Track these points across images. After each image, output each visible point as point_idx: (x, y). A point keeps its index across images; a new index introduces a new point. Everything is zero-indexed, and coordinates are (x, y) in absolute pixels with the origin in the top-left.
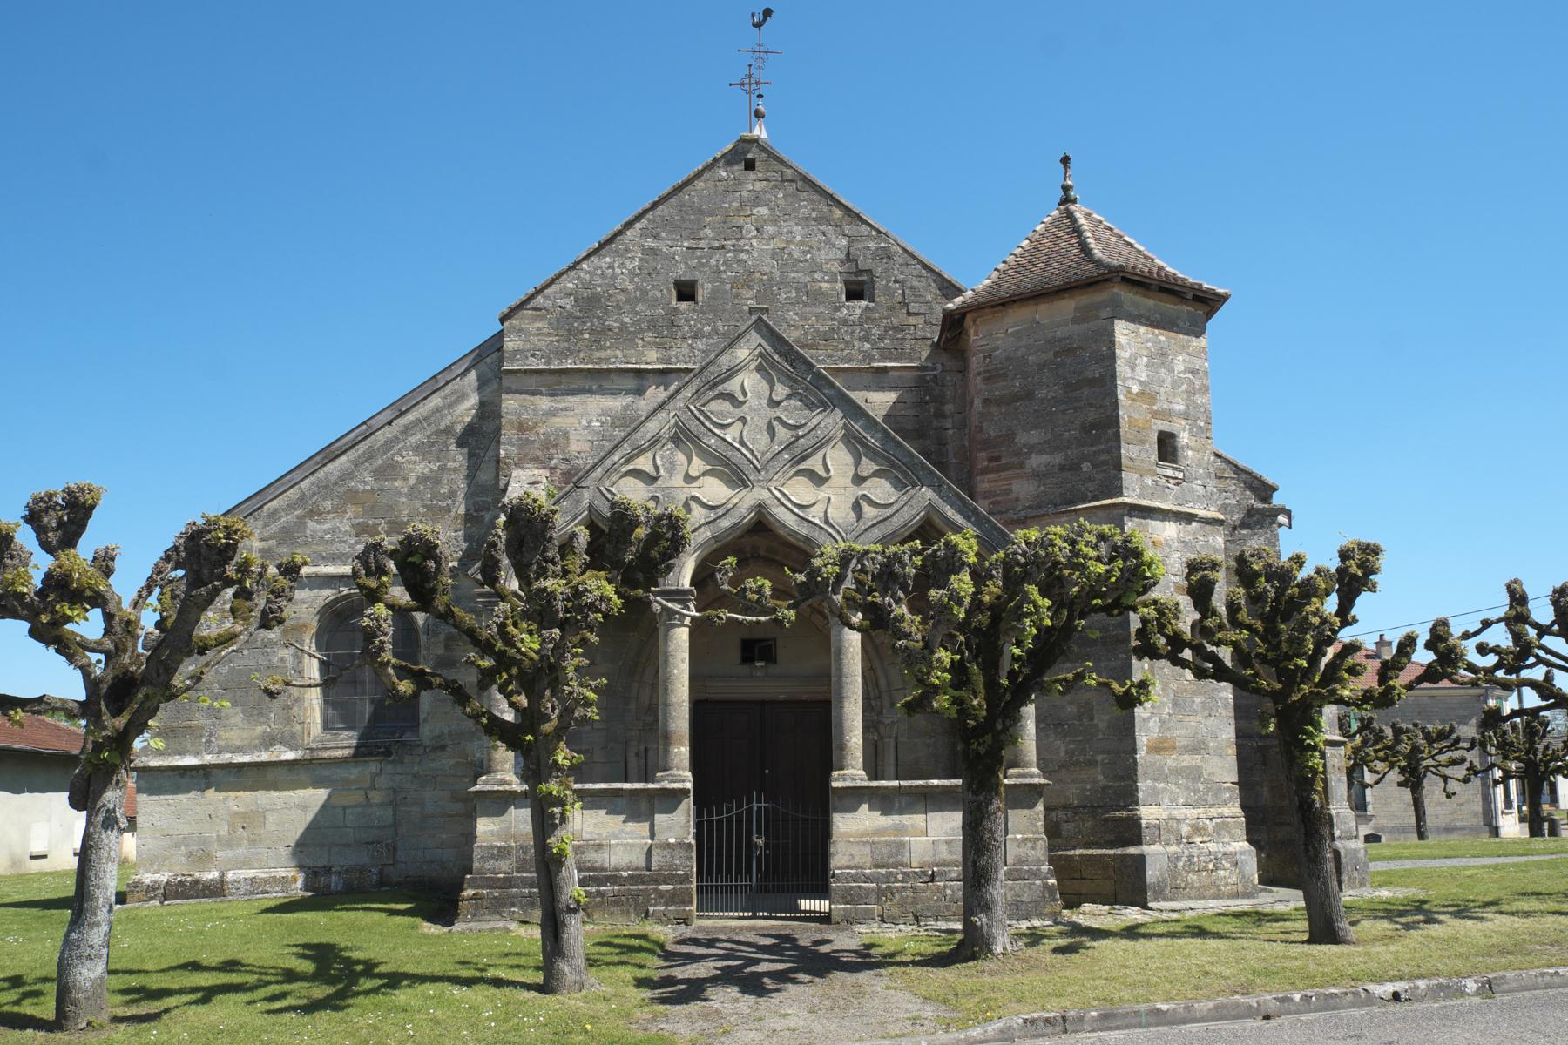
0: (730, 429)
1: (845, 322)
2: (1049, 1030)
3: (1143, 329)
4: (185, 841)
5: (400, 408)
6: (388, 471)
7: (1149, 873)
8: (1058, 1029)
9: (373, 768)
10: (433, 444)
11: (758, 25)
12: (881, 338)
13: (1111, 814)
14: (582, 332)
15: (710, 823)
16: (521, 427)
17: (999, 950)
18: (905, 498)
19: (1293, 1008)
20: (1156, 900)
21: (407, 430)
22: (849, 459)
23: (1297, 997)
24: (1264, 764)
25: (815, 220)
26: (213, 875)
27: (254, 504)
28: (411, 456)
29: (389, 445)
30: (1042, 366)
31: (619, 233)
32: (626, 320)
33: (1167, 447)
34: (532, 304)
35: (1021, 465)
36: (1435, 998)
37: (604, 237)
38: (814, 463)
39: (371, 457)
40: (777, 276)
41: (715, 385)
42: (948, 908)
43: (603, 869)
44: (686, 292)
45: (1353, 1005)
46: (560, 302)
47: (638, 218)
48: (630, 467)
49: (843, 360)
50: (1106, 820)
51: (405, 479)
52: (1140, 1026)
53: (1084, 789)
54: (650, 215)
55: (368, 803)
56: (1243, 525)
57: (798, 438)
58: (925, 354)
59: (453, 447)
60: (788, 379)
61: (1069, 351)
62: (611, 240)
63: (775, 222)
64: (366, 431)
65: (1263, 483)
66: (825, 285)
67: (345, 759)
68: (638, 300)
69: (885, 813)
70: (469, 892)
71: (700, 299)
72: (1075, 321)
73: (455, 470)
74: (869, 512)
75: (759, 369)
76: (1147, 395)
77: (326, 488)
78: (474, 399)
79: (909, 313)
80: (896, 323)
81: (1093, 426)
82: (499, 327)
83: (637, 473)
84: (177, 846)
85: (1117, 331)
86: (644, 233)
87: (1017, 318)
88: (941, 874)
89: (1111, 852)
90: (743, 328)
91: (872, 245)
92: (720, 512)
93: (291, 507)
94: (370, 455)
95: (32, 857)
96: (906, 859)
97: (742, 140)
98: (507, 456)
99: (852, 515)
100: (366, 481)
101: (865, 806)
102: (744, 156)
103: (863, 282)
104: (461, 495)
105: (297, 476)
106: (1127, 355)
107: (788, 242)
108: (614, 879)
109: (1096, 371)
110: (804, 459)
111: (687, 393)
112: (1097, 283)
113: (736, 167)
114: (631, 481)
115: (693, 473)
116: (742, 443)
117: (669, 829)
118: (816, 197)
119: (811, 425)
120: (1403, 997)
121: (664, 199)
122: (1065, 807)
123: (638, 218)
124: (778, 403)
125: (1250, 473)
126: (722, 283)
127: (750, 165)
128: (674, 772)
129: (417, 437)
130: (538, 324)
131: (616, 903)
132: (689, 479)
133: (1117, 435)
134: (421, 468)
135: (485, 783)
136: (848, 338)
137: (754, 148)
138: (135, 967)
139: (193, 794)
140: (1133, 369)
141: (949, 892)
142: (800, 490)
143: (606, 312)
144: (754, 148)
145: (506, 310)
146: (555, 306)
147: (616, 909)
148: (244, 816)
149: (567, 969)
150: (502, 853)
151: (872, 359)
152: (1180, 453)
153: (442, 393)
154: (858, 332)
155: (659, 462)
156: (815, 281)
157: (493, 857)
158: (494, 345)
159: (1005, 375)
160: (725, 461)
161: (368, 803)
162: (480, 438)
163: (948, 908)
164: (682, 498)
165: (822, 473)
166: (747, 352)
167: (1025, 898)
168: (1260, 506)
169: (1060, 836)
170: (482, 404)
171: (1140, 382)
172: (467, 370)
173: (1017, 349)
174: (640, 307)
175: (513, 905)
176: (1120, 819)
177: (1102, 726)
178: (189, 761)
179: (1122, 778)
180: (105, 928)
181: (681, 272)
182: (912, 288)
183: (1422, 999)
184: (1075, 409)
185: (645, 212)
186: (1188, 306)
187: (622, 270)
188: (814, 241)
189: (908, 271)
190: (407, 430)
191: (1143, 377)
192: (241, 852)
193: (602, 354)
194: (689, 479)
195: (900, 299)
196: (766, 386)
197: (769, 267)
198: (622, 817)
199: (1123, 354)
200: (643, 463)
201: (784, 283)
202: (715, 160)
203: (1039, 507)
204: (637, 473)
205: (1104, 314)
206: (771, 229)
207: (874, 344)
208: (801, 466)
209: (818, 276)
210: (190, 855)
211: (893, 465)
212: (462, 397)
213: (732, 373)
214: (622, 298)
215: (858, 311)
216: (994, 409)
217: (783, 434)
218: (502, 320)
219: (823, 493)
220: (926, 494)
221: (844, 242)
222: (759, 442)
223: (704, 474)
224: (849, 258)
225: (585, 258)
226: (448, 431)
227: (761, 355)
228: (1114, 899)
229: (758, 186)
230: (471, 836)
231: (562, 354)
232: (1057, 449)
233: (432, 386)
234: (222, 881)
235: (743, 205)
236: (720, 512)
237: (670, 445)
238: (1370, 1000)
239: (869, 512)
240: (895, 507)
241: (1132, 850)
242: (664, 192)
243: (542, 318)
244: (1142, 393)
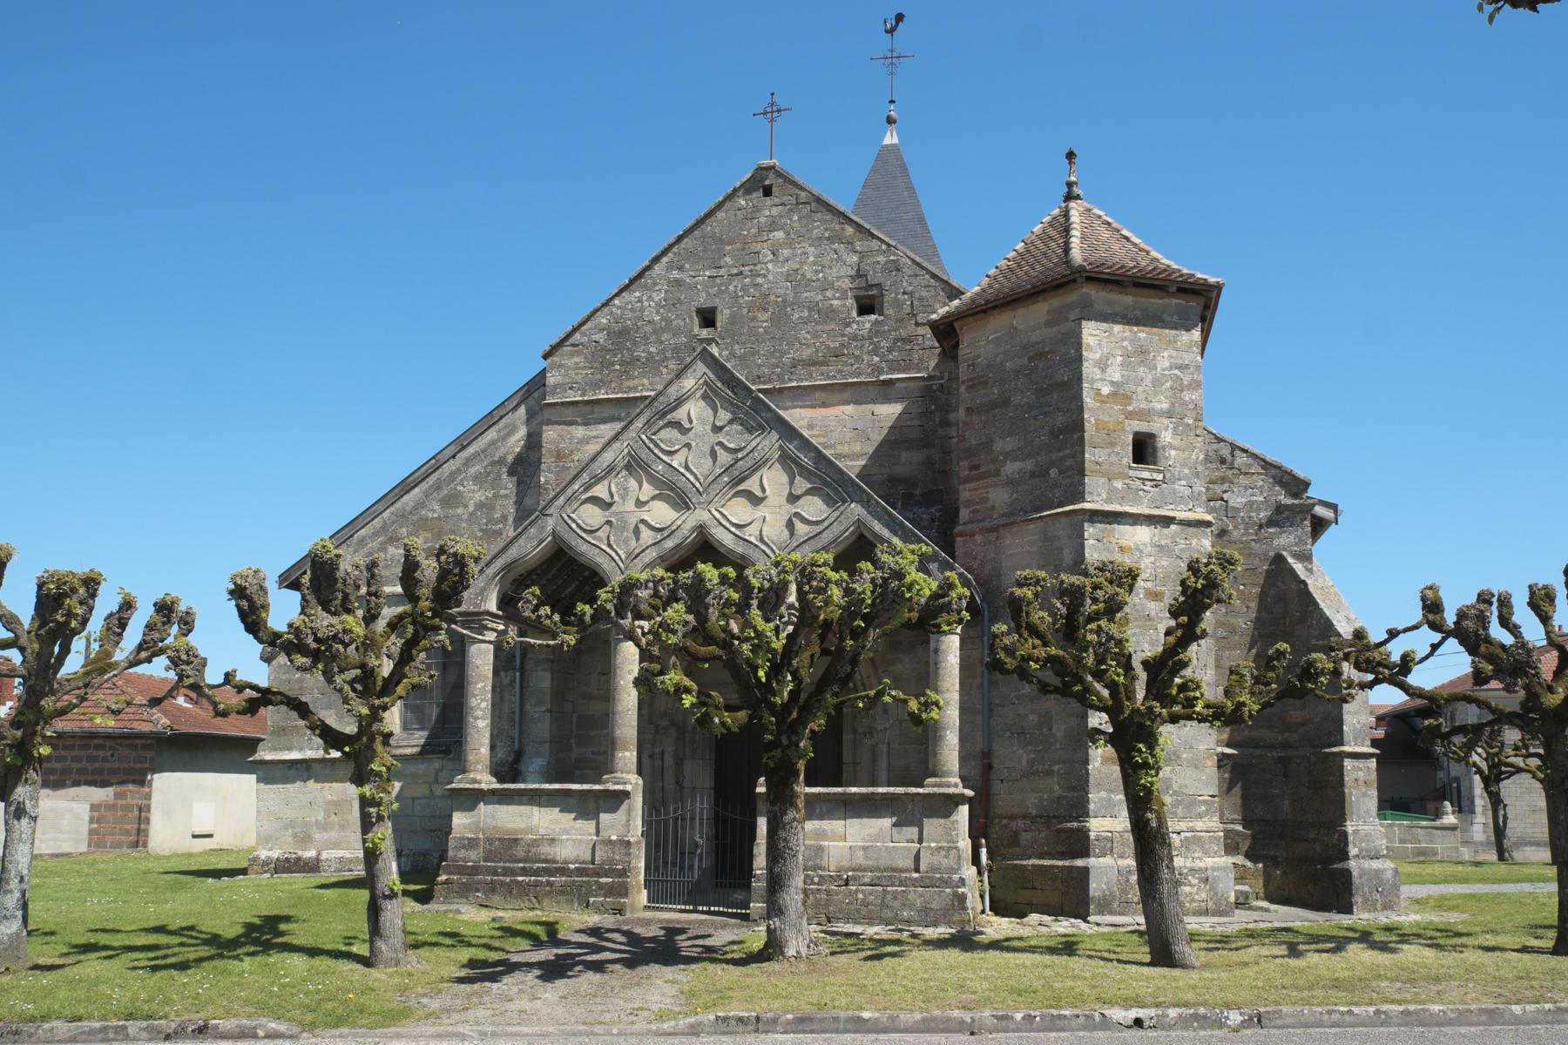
0: (677, 456)
1: (855, 338)
2: (741, 1028)
3: (1117, 328)
4: (291, 824)
5: (462, 442)
6: (453, 500)
7: (1093, 886)
8: (750, 1028)
9: (437, 764)
10: (488, 474)
11: (891, 31)
12: (890, 351)
13: (1064, 825)
14: (613, 364)
15: (658, 822)
16: (559, 456)
17: (791, 952)
18: (836, 514)
19: (1011, 1026)
20: (1101, 913)
21: (467, 463)
22: (785, 479)
23: (1019, 1016)
24: (1286, 775)
25: (828, 239)
26: (310, 854)
27: (344, 535)
28: (471, 486)
29: (453, 476)
30: (1017, 372)
31: (648, 268)
32: (653, 349)
33: (1144, 449)
34: (571, 341)
35: (997, 473)
36: (1185, 1028)
37: (634, 273)
38: (751, 485)
39: (439, 488)
40: (790, 298)
41: (664, 415)
42: (858, 911)
43: (555, 862)
44: (707, 318)
45: (1084, 1028)
46: (595, 337)
47: (664, 252)
48: (589, 494)
49: (852, 375)
50: (1059, 831)
51: (466, 506)
52: (837, 1031)
53: (1041, 799)
54: (675, 249)
55: (432, 796)
56: (1271, 522)
57: (737, 460)
58: (933, 364)
59: (504, 476)
60: (729, 405)
61: (1041, 355)
62: (640, 275)
63: (790, 245)
64: (435, 464)
65: (1295, 478)
66: (835, 303)
67: (413, 756)
68: (663, 330)
70: (443, 878)
71: (719, 324)
72: (1048, 324)
73: (506, 496)
74: (801, 529)
75: (705, 397)
76: (1120, 395)
77: (402, 517)
78: (522, 432)
79: (917, 324)
80: (904, 333)
81: (1061, 431)
82: (544, 364)
83: (595, 500)
84: (286, 828)
85: (1085, 332)
86: (670, 268)
87: (997, 324)
88: (855, 878)
89: (1060, 863)
90: (688, 360)
91: (881, 259)
92: (666, 533)
93: (375, 534)
94: (437, 487)
95: (194, 836)
96: (824, 863)
97: (760, 169)
98: (547, 483)
99: (786, 532)
100: (435, 510)
102: (762, 183)
103: (873, 297)
104: (511, 519)
105: (380, 507)
106: (1097, 356)
107: (802, 263)
108: (562, 871)
109: (1064, 375)
110: (742, 480)
111: (639, 424)
112: (1044, 291)
113: (755, 195)
114: (589, 507)
115: (643, 499)
116: (687, 468)
117: (612, 827)
118: (829, 217)
119: (749, 448)
120: (1146, 1024)
121: (688, 232)
122: (1024, 817)
123: (664, 252)
124: (721, 428)
125: (1280, 468)
126: (740, 308)
127: (768, 192)
128: (618, 775)
129: (476, 469)
130: (576, 359)
131: (562, 893)
132: (640, 504)
133: (1082, 438)
134: (479, 496)
135: (460, 781)
136: (857, 353)
137: (772, 175)
138: (110, 926)
139: (298, 784)
140: (1103, 371)
141: (860, 896)
142: (738, 511)
143: (635, 344)
144: (772, 175)
145: (547, 348)
146: (590, 341)
147: (562, 898)
148: (336, 804)
149: (384, 947)
150: (472, 843)
151: (881, 371)
152: (1160, 454)
153: (496, 427)
154: (868, 346)
155: (614, 489)
156: (826, 299)
157: (464, 847)
158: (537, 384)
159: (986, 383)
160: (671, 486)
161: (432, 796)
162: (525, 466)
163: (858, 911)
164: (633, 520)
165: (759, 493)
166: (693, 382)
168: (1289, 501)
169: (1018, 845)
170: (530, 435)
171: (1112, 383)
172: (518, 405)
173: (996, 356)
174: (665, 337)
176: (1071, 830)
177: (1059, 735)
178: (295, 755)
179: (1074, 789)
180: (17, 895)
181: (703, 301)
182: (921, 299)
183: (1170, 1027)
184: (1045, 414)
185: (671, 246)
186: (1192, 302)
187: (649, 303)
188: (826, 261)
189: (916, 282)
190: (467, 463)
191: (1117, 377)
192: (333, 834)
193: (631, 383)
194: (640, 504)
195: (908, 310)
196: (711, 412)
197: (784, 289)
198: (573, 815)
199: (1091, 356)
200: (600, 491)
201: (798, 304)
202: (735, 190)
203: (1012, 514)
204: (595, 500)
205: (1073, 316)
206: (786, 252)
207: (882, 357)
208: (740, 488)
209: (829, 294)
210: (295, 835)
211: (826, 484)
212: (514, 429)
213: (680, 402)
214: (649, 329)
215: (868, 325)
216: (975, 418)
217: (725, 458)
218: (545, 357)
219: (759, 512)
220: (856, 510)
221: (855, 259)
222: (702, 466)
223: (653, 498)
224: (860, 274)
225: (617, 295)
226: (501, 462)
227: (706, 383)
228: (1058, 911)
229: (775, 211)
230: (448, 830)
231: (597, 385)
232: (1029, 455)
233: (489, 421)
234: (318, 859)
235: (760, 231)
236: (666, 533)
237: (624, 473)
238: (1106, 1023)
239: (801, 529)
240: (826, 524)
241: (1080, 863)
242: (688, 225)
243: (579, 353)
244: (1114, 395)
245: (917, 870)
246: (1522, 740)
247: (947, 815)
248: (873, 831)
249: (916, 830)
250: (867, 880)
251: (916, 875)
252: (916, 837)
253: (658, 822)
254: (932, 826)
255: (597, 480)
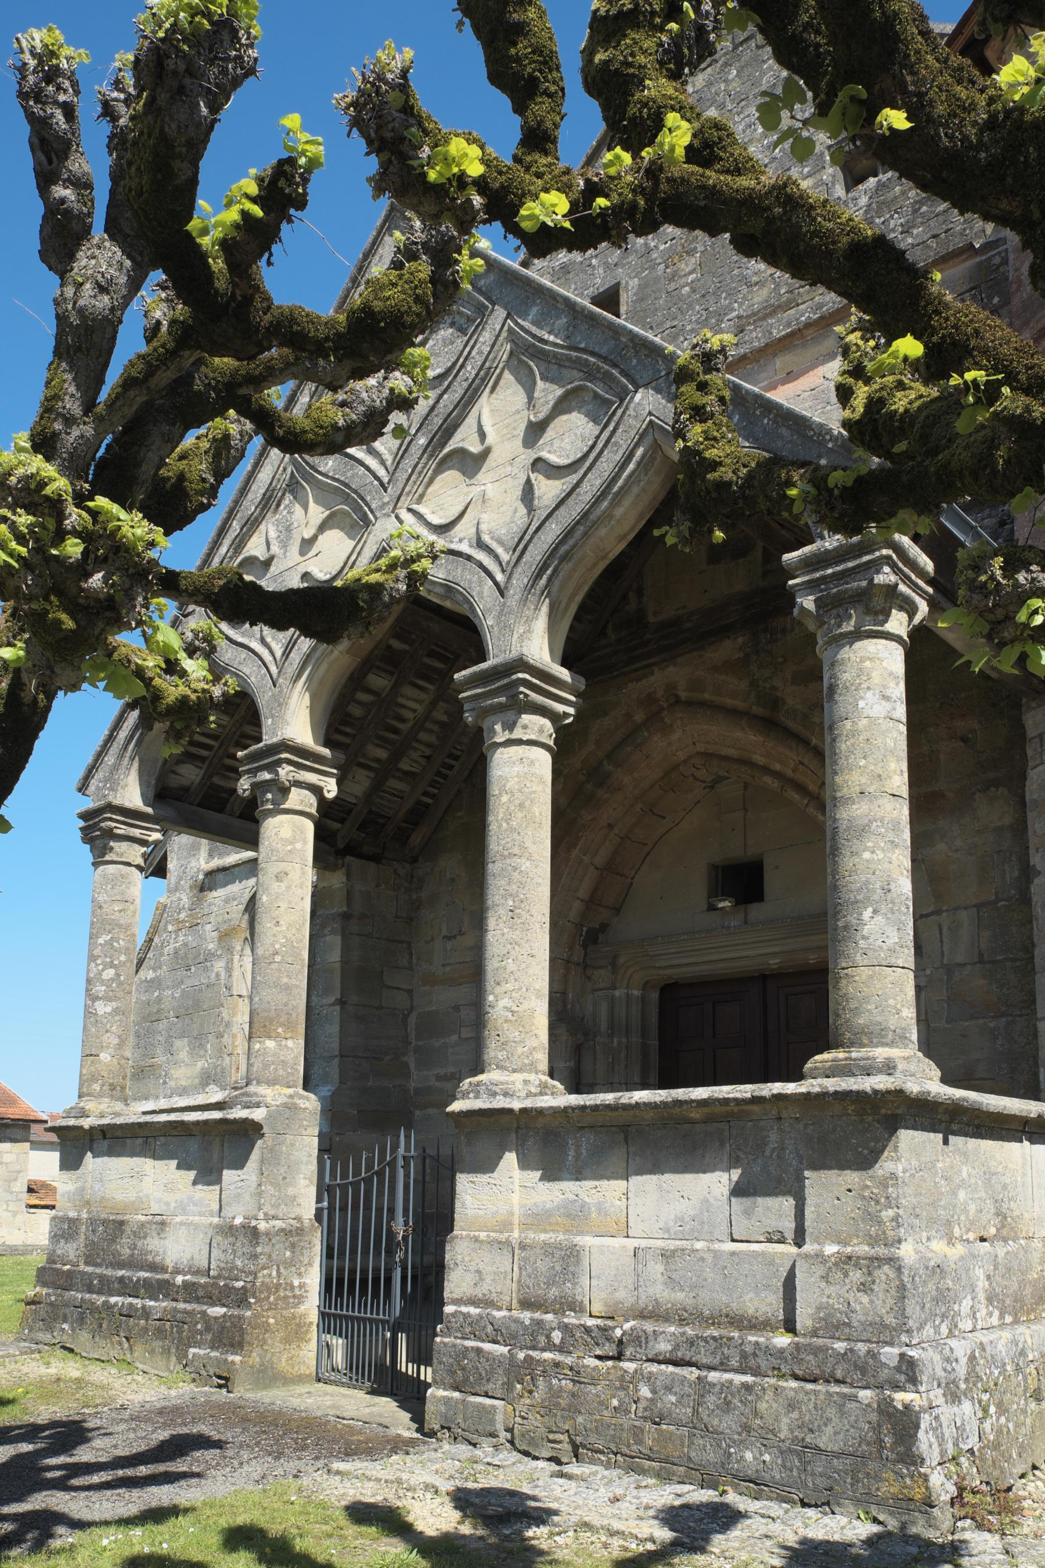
38: (465, 438)
69: (550, 1175)
88: (638, 1339)
99: (523, 510)
101: (510, 1158)
131: (160, 1333)
141: (645, 1392)
163: (637, 1434)
165: (475, 448)
167: (824, 1440)
175: (65, 1321)
211: (591, 373)
237: (288, 498)
239: (548, 490)
245: (790, 1326)
246: (788, 83)
247: (866, 1161)
248: (685, 1208)
249: (788, 1204)
250: (663, 1347)
251: (782, 1340)
252: (789, 1226)
253: (344, 1188)
254: (828, 1190)
255: (252, 525)
